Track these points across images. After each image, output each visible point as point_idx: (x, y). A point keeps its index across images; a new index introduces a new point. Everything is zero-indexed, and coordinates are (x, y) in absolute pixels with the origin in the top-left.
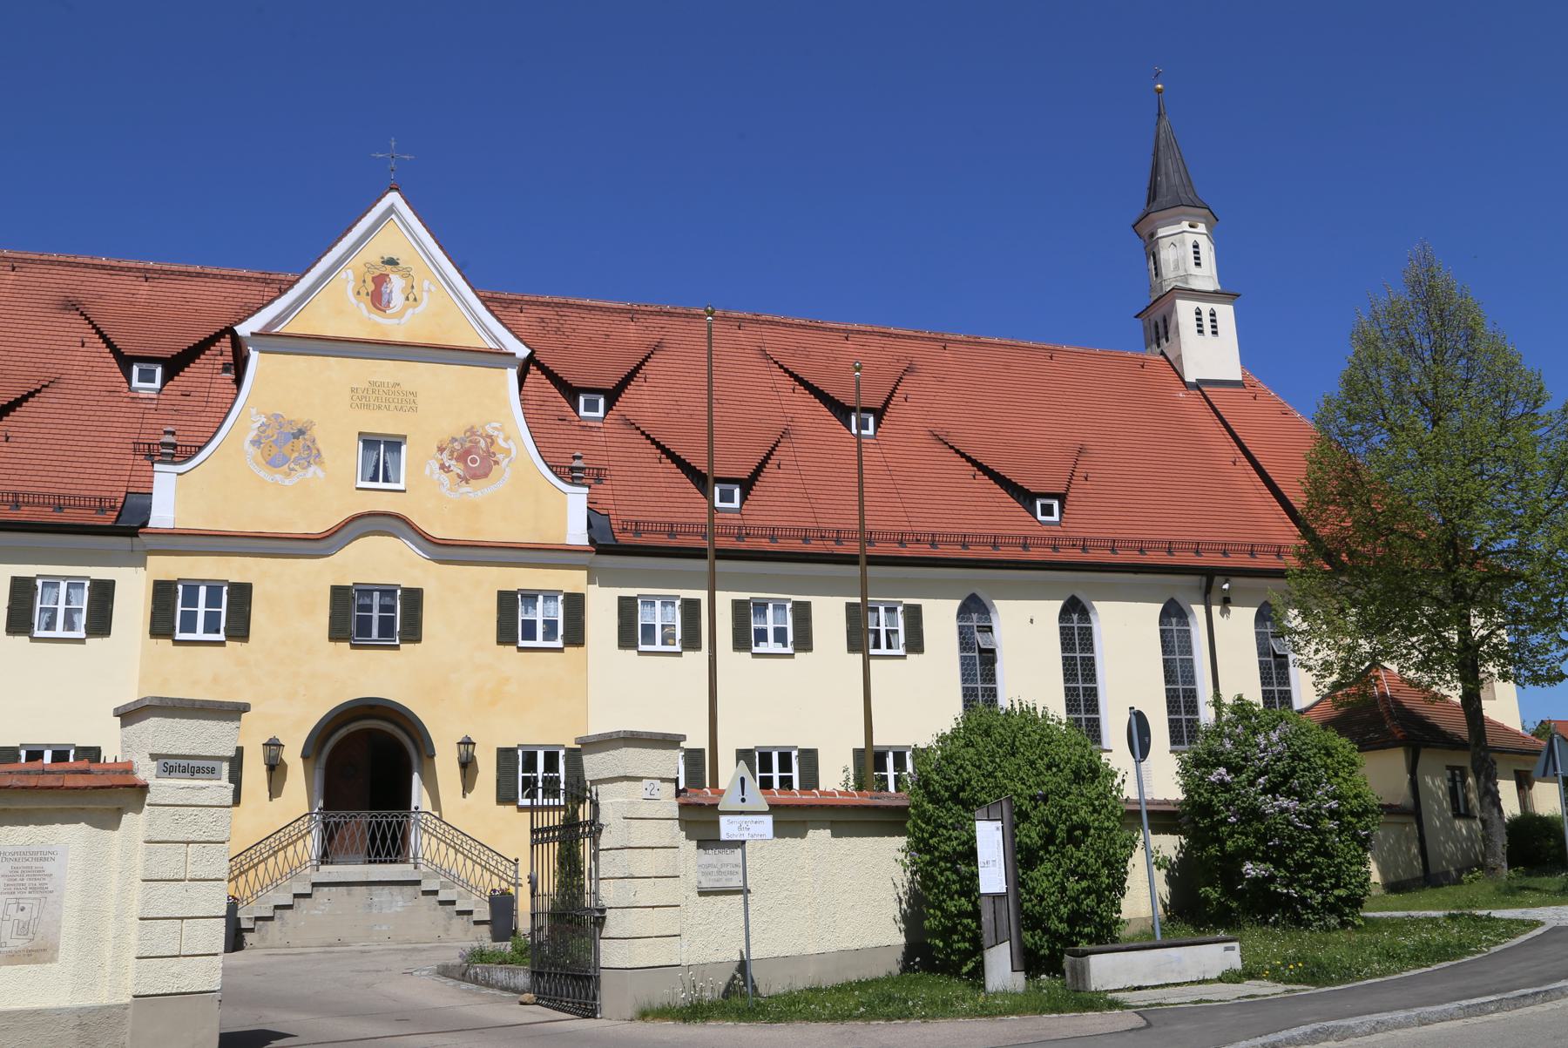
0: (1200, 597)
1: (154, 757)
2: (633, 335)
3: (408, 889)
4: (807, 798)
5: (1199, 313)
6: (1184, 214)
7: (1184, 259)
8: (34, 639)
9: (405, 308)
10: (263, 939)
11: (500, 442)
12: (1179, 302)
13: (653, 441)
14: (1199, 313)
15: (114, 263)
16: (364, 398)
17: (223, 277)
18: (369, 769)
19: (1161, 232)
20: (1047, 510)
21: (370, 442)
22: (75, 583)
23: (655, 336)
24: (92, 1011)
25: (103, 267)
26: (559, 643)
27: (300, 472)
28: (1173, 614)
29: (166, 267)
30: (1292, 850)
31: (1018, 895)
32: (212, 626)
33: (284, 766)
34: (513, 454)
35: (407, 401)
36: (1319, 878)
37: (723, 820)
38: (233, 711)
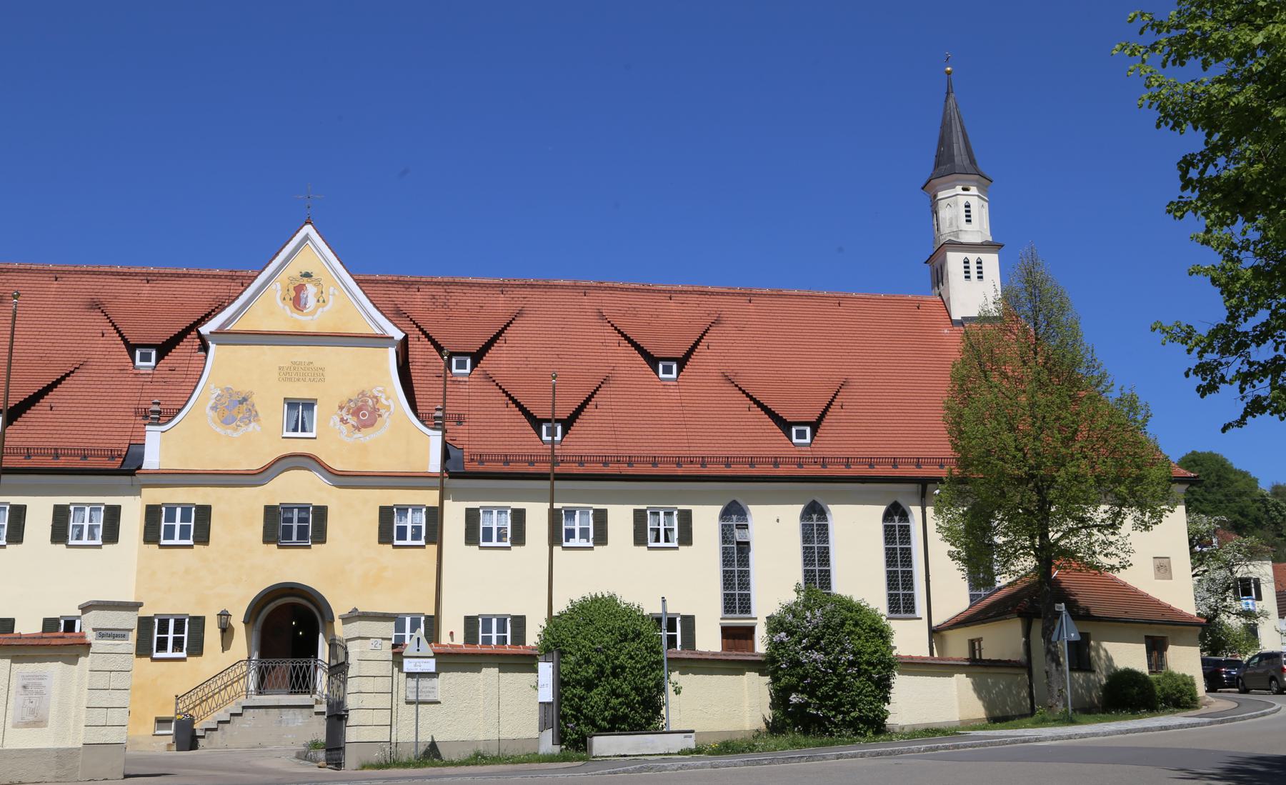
0: (918, 499)
1: (94, 630)
2: (500, 305)
3: (306, 711)
4: (687, 655)
5: (967, 262)
6: (957, 180)
7: (957, 217)
8: (69, 546)
9: (317, 308)
10: (210, 743)
11: (383, 401)
12: (949, 254)
13: (504, 392)
14: (967, 262)
15: (126, 270)
17: (202, 276)
18: (290, 630)
19: (941, 195)
20: (801, 435)
21: (292, 404)
22: (95, 508)
23: (519, 305)
24: (63, 750)
25: (118, 274)
26: (422, 542)
27: (244, 428)
28: (896, 513)
29: (162, 271)
30: (821, 686)
31: (560, 704)
32: (184, 535)
33: (232, 629)
35: (318, 375)
36: (841, 704)
37: (405, 661)
38: (135, 606)
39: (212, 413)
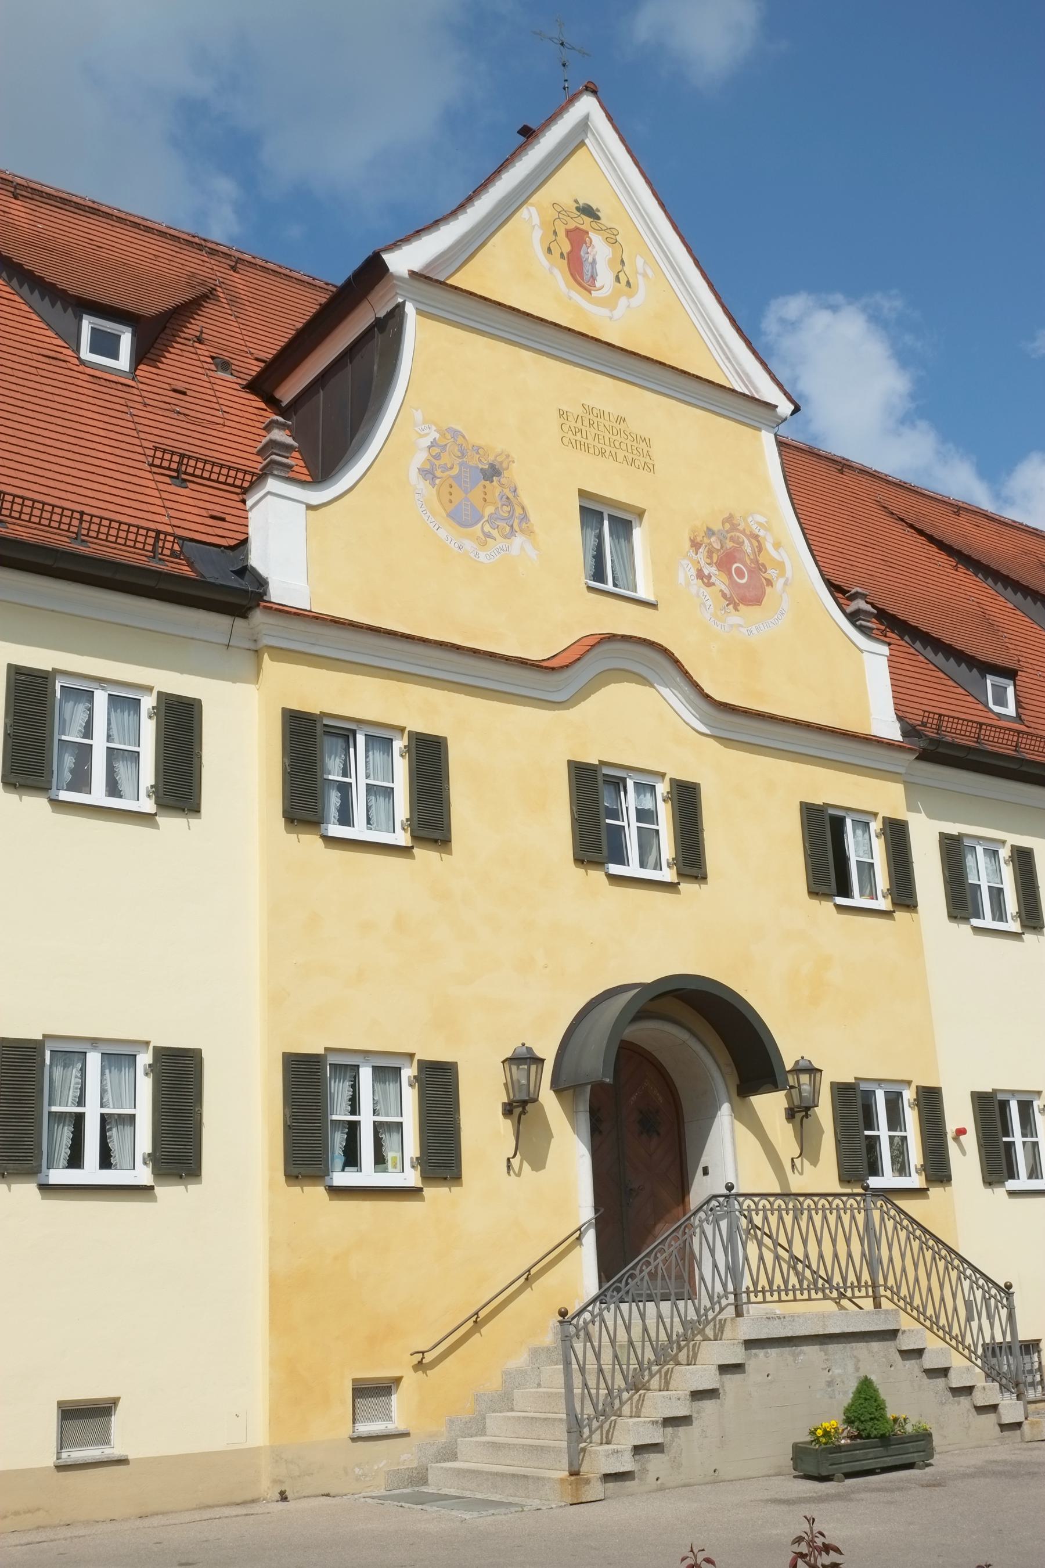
9: (615, 296)
11: (769, 546)
16: (583, 431)
34: (789, 573)
35: (638, 454)
39: (423, 486)
